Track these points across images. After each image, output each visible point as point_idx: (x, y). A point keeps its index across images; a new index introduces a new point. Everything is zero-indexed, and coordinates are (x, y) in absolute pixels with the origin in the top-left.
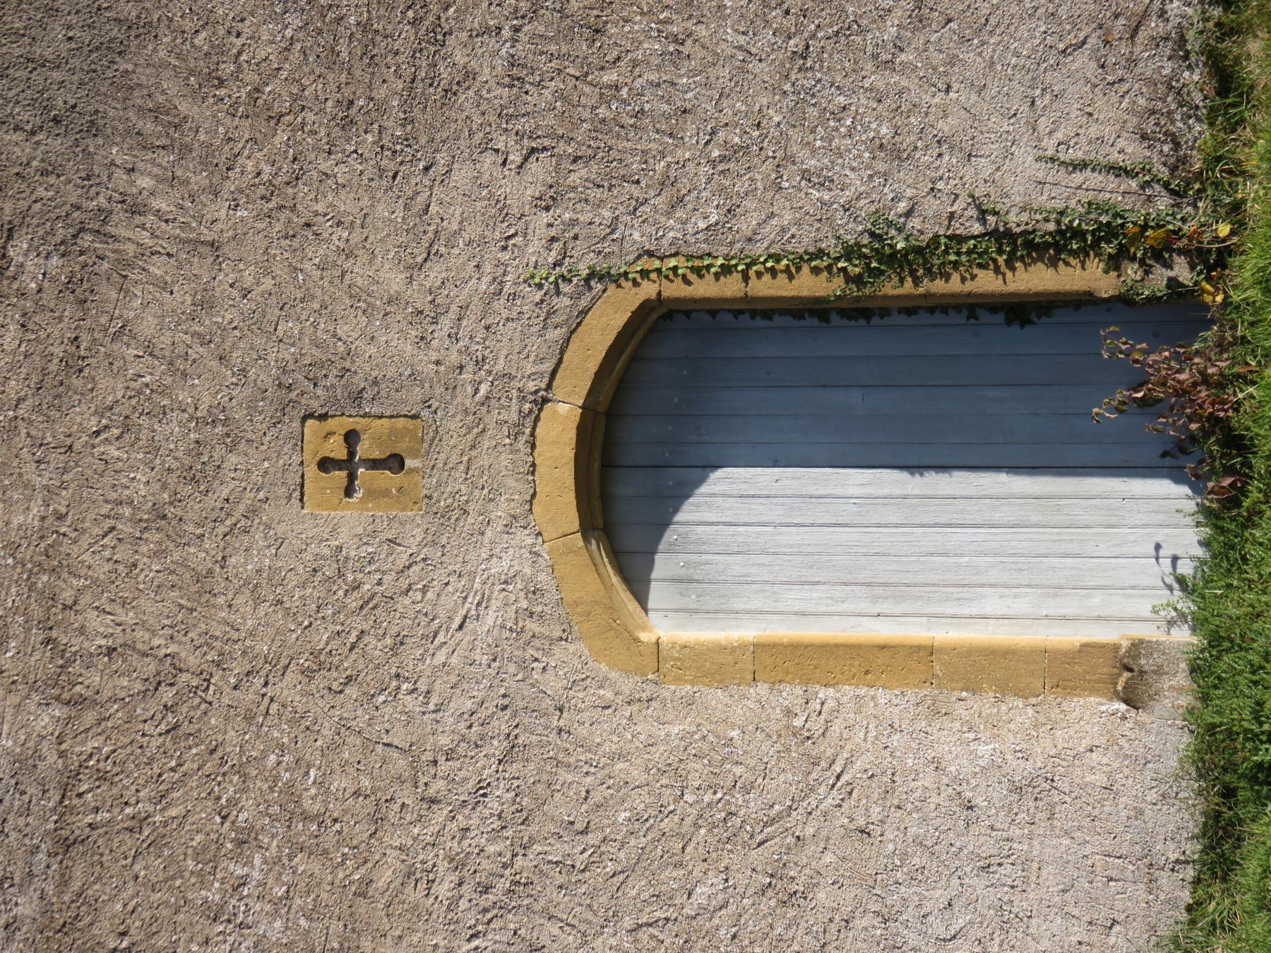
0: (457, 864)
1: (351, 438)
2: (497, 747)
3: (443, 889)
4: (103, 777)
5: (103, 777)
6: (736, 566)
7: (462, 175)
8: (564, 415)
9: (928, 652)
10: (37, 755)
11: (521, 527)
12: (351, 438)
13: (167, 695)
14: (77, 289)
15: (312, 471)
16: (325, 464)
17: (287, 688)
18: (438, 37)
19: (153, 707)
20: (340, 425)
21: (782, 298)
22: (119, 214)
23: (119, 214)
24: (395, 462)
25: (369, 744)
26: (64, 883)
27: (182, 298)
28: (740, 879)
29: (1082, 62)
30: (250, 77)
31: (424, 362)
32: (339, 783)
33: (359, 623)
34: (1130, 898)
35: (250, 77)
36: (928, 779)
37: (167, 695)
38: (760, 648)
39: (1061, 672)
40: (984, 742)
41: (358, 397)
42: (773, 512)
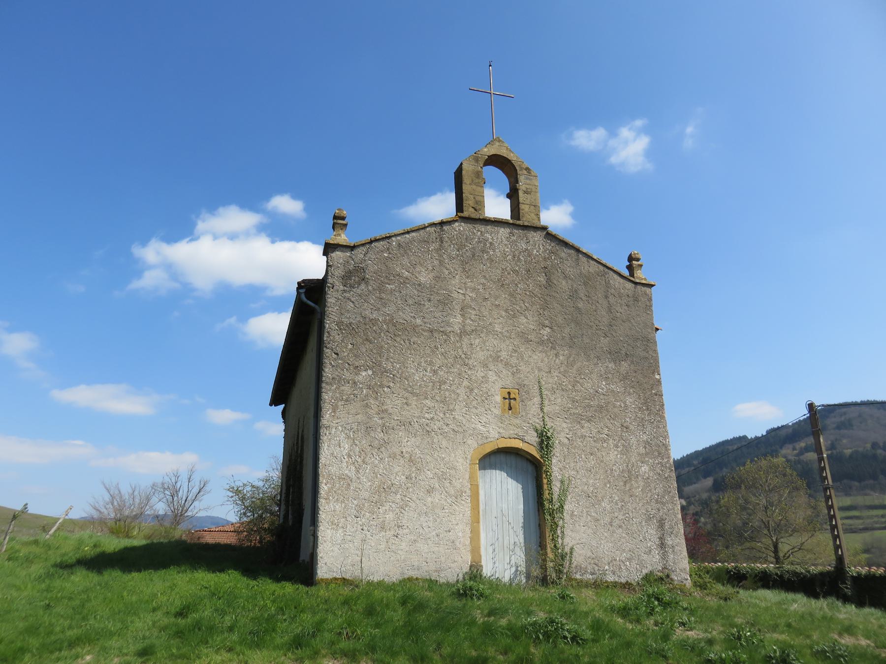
0: (432, 419)
1: (515, 399)
2: (456, 429)
3: (426, 415)
4: (446, 341)
5: (446, 341)
6: (488, 480)
7: (564, 425)
8: (519, 445)
9: (478, 522)
10: (450, 326)
11: (497, 432)
12: (515, 399)
13: (463, 356)
14: (541, 342)
15: (508, 390)
16: (509, 393)
17: (466, 383)
18: (589, 421)
19: (461, 353)
20: (517, 397)
21: (314, 521)
22: (555, 352)
23: (555, 352)
24: (510, 409)
25: (455, 400)
26: (423, 330)
27: (540, 364)
28: (432, 481)
29: (589, 554)
30: (581, 381)
31: (530, 416)
32: (447, 393)
33: (479, 399)
34: (432, 567)
35: (581, 381)
36: (454, 522)
37: (463, 356)
38: (477, 486)
39: (475, 550)
40: (462, 532)
41: (522, 401)
42: (499, 489)
